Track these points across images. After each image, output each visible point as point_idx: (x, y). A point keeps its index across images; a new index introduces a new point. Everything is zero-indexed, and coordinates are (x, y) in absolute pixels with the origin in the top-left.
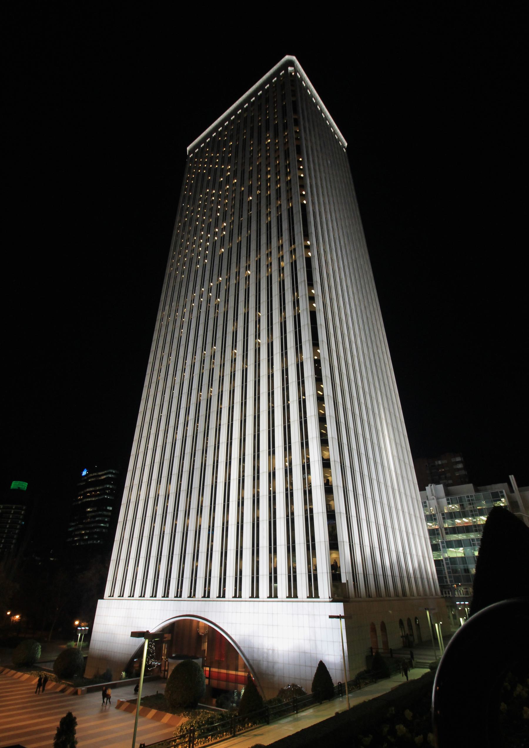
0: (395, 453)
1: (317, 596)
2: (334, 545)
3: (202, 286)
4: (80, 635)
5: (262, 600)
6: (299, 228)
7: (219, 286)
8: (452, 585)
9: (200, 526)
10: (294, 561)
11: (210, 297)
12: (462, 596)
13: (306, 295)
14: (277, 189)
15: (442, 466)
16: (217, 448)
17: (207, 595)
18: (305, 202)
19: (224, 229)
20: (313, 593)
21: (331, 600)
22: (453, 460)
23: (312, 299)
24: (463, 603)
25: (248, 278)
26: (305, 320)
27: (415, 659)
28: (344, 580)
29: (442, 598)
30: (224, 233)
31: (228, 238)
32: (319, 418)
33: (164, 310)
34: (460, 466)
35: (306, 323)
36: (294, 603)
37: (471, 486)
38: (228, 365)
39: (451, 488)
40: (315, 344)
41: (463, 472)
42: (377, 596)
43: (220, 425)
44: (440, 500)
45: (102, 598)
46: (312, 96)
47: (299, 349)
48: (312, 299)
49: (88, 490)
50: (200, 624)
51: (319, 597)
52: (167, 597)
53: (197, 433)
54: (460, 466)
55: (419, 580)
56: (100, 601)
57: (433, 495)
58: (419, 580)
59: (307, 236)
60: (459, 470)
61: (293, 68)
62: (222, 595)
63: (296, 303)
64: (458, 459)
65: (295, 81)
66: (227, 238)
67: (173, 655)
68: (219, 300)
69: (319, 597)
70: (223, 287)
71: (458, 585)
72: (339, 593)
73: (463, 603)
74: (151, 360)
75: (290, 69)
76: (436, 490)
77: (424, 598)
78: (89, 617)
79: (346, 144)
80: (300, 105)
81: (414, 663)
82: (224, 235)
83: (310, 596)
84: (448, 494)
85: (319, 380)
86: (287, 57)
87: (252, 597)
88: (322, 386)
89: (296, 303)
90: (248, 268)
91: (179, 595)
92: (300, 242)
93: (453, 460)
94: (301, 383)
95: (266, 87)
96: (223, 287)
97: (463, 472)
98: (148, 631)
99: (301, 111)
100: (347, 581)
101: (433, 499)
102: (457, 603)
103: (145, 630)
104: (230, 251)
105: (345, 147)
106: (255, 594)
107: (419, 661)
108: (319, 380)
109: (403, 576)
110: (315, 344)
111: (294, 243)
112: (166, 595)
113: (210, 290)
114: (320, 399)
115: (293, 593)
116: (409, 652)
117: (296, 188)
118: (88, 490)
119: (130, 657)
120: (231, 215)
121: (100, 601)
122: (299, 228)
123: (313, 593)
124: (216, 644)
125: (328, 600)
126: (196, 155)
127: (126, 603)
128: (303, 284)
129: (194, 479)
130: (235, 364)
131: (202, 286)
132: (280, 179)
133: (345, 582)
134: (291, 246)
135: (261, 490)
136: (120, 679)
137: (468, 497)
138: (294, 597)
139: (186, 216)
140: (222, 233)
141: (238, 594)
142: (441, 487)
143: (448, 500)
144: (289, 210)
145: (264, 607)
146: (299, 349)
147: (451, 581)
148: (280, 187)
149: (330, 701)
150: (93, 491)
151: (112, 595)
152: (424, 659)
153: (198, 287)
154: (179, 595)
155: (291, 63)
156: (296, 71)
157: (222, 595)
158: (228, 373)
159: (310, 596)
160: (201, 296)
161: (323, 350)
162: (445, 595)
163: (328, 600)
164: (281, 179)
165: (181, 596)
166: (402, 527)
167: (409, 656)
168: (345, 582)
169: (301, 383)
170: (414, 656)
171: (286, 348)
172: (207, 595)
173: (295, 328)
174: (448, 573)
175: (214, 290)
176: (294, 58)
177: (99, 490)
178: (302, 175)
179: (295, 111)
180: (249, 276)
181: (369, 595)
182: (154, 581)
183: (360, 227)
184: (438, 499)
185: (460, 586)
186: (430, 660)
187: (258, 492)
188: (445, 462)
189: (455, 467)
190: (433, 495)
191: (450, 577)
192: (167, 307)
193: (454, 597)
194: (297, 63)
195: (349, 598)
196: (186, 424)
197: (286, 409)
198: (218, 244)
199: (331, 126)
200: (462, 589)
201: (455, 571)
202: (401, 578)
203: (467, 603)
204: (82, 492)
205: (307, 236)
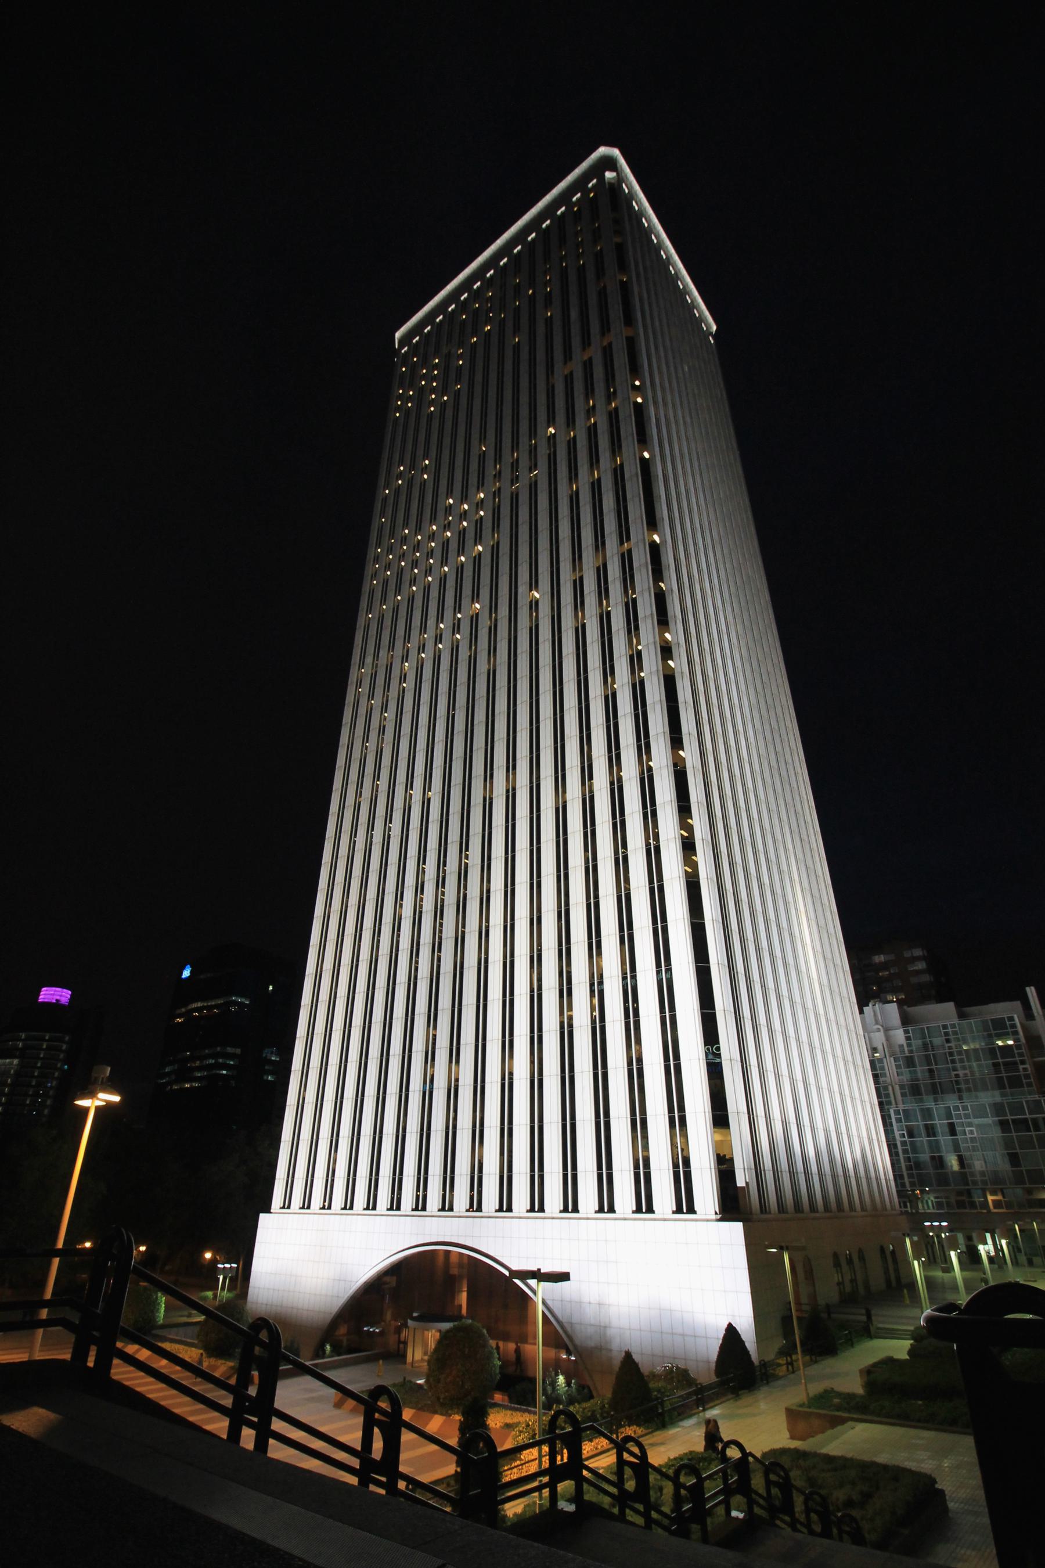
0: (818, 947)
1: (691, 1210)
2: (720, 1118)
3: (440, 618)
4: (221, 1277)
5: (585, 1216)
6: (636, 511)
7: (475, 619)
8: (913, 1191)
9: (457, 1080)
10: (646, 1147)
11: (458, 641)
12: (931, 1211)
13: (655, 643)
14: (589, 428)
15: (884, 966)
16: (484, 934)
17: (476, 1205)
18: (646, 455)
19: (480, 504)
20: (685, 1204)
21: (719, 1217)
22: (907, 954)
23: (666, 651)
24: (936, 1224)
25: (534, 605)
26: (655, 694)
27: (875, 1323)
28: (740, 1182)
29: (902, 1213)
30: (482, 513)
31: (490, 524)
32: (687, 882)
33: (362, 664)
34: (921, 966)
35: (657, 698)
36: (571, 1221)
37: (951, 1006)
38: (501, 778)
39: (916, 1010)
40: (676, 741)
41: (926, 978)
42: (779, 1211)
43: (488, 891)
44: (892, 1033)
45: (267, 1210)
46: (650, 230)
47: (644, 748)
48: (666, 651)
49: (194, 1005)
50: (454, 1259)
51: (694, 1212)
52: (374, 1208)
53: (442, 906)
54: (921, 966)
55: (769, 1176)
56: (263, 1217)
57: (877, 1023)
58: (769, 1176)
59: (652, 524)
60: (918, 973)
61: (614, 174)
62: (505, 1205)
63: (636, 660)
64: (918, 952)
65: (615, 193)
66: (488, 525)
67: (415, 1315)
68: (458, 636)
69: (694, 1212)
70: (484, 623)
71: (923, 1192)
72: (731, 1203)
73: (936, 1224)
74: (340, 762)
75: (609, 175)
76: (882, 1013)
77: (876, 1212)
78: (242, 1247)
79: (714, 328)
80: (631, 253)
81: (872, 1329)
82: (481, 517)
83: (679, 1210)
84: (906, 1020)
85: (684, 808)
86: (602, 150)
87: (532, 1209)
88: (689, 821)
89: (636, 660)
90: (534, 584)
91: (420, 1205)
92: (640, 537)
93: (907, 954)
94: (650, 814)
95: (559, 213)
96: (484, 623)
97: (926, 978)
98: (539, 1270)
99: (633, 267)
100: (747, 1183)
101: (878, 1030)
102: (927, 1224)
103: (535, 1269)
104: (495, 550)
105: (711, 334)
106: (606, 1205)
107: (881, 1326)
108: (684, 808)
109: (838, 1173)
110: (676, 741)
111: (628, 539)
112: (395, 1205)
113: (456, 627)
114: (688, 846)
115: (644, 1204)
116: (864, 1311)
117: (628, 429)
118: (194, 1005)
119: (329, 1318)
120: (495, 476)
121: (263, 1217)
122: (636, 511)
123: (685, 1204)
124: (498, 1293)
125: (714, 1217)
126: (415, 350)
127: (314, 1221)
128: (649, 621)
129: (444, 995)
130: (514, 774)
131: (440, 618)
132: (594, 406)
133: (744, 1185)
134: (622, 543)
135: (575, 1013)
136: (323, 1358)
137: (945, 1027)
138: (573, 1212)
139: (400, 475)
140: (477, 512)
141: (537, 1205)
142: (893, 1009)
143: (906, 1032)
144: (615, 470)
145: (625, 1227)
146: (644, 748)
147: (912, 1184)
148: (595, 423)
149: (750, 1391)
150: (203, 1008)
151: (287, 1205)
152: (903, 1324)
153: (431, 622)
154: (420, 1205)
155: (609, 163)
156: (620, 179)
157: (505, 1205)
158: (501, 792)
159: (679, 1210)
160: (438, 638)
161: (690, 754)
162: (903, 1209)
163: (714, 1217)
164: (598, 406)
165: (424, 1209)
166: (825, 1082)
167: (864, 1318)
168: (744, 1185)
169: (650, 814)
170: (873, 1318)
171: (618, 747)
172: (476, 1205)
173: (636, 708)
174: (907, 1169)
175: (465, 627)
176: (616, 152)
177: (216, 1006)
178: (639, 400)
179: (623, 267)
180: (537, 602)
181: (781, 1207)
182: (370, 1180)
183: (743, 500)
184: (887, 1030)
185: (928, 1192)
186: (908, 1324)
187: (570, 1018)
188: (892, 957)
189: (912, 968)
190: (877, 1023)
191: (910, 1176)
192: (369, 660)
193: (917, 1212)
194: (622, 162)
195: (751, 1213)
196: (420, 888)
197: (621, 863)
198: (470, 535)
199: (686, 291)
200: (931, 1199)
201: (918, 1165)
202: (834, 1176)
203: (944, 1224)
204: (183, 1010)
205: (652, 524)
